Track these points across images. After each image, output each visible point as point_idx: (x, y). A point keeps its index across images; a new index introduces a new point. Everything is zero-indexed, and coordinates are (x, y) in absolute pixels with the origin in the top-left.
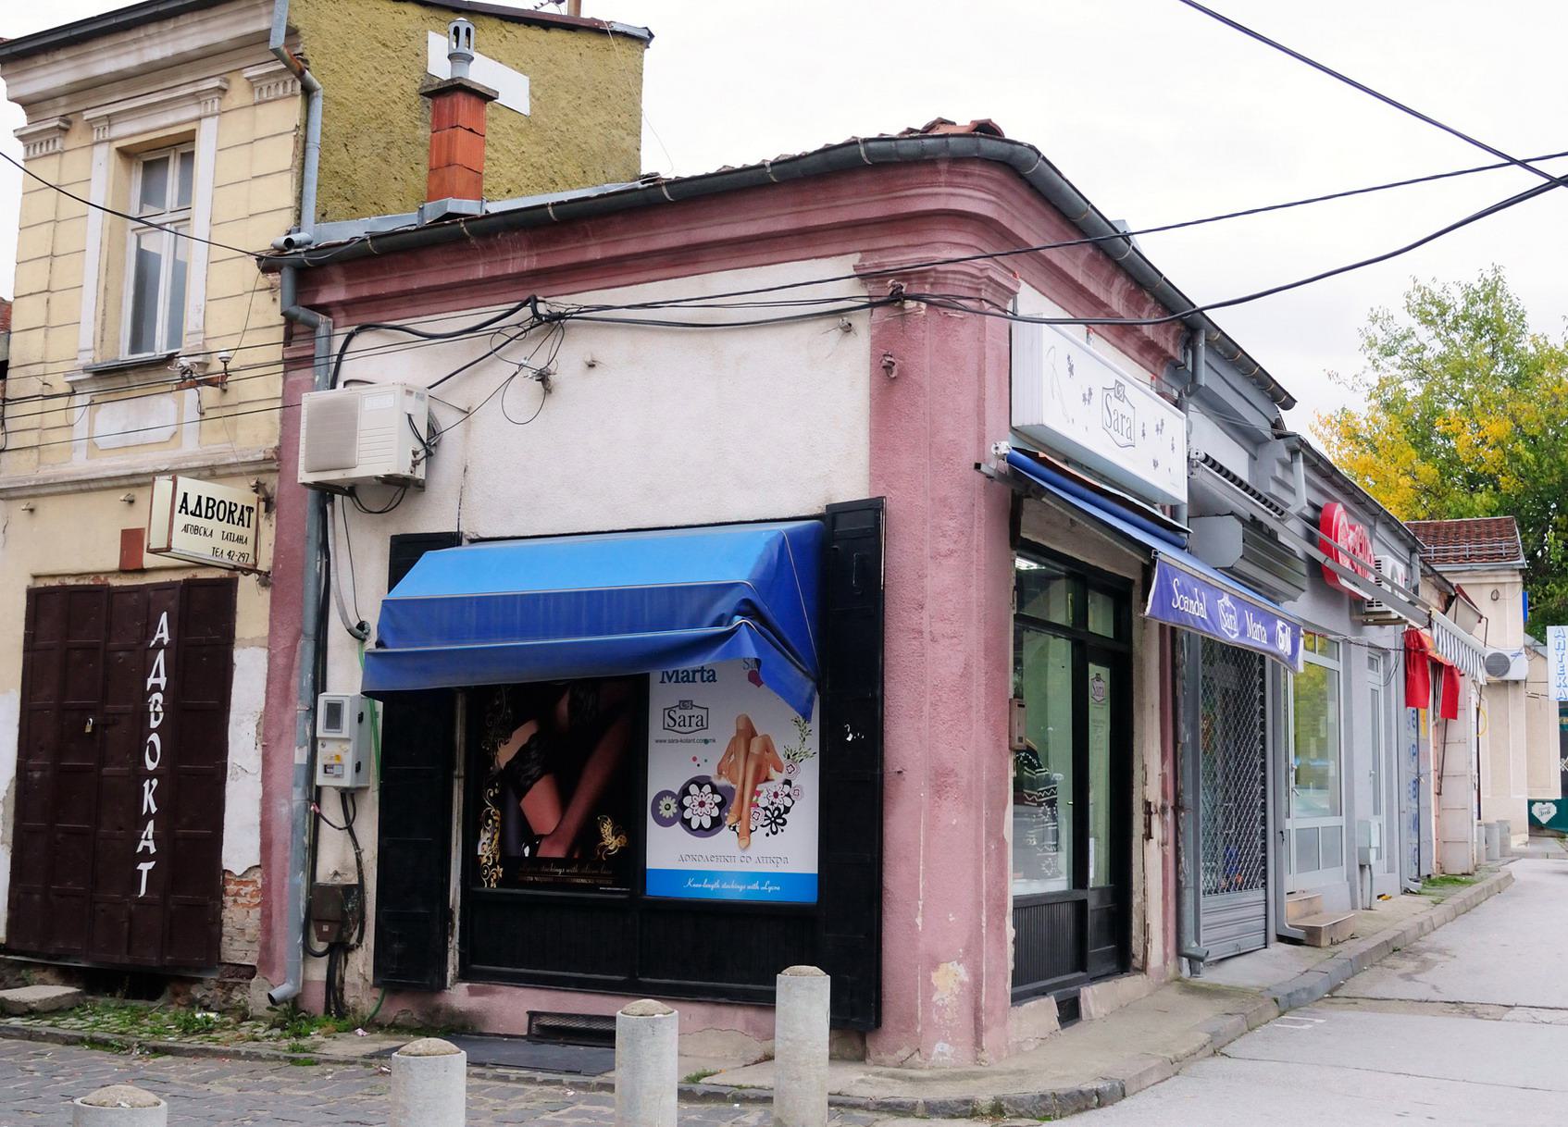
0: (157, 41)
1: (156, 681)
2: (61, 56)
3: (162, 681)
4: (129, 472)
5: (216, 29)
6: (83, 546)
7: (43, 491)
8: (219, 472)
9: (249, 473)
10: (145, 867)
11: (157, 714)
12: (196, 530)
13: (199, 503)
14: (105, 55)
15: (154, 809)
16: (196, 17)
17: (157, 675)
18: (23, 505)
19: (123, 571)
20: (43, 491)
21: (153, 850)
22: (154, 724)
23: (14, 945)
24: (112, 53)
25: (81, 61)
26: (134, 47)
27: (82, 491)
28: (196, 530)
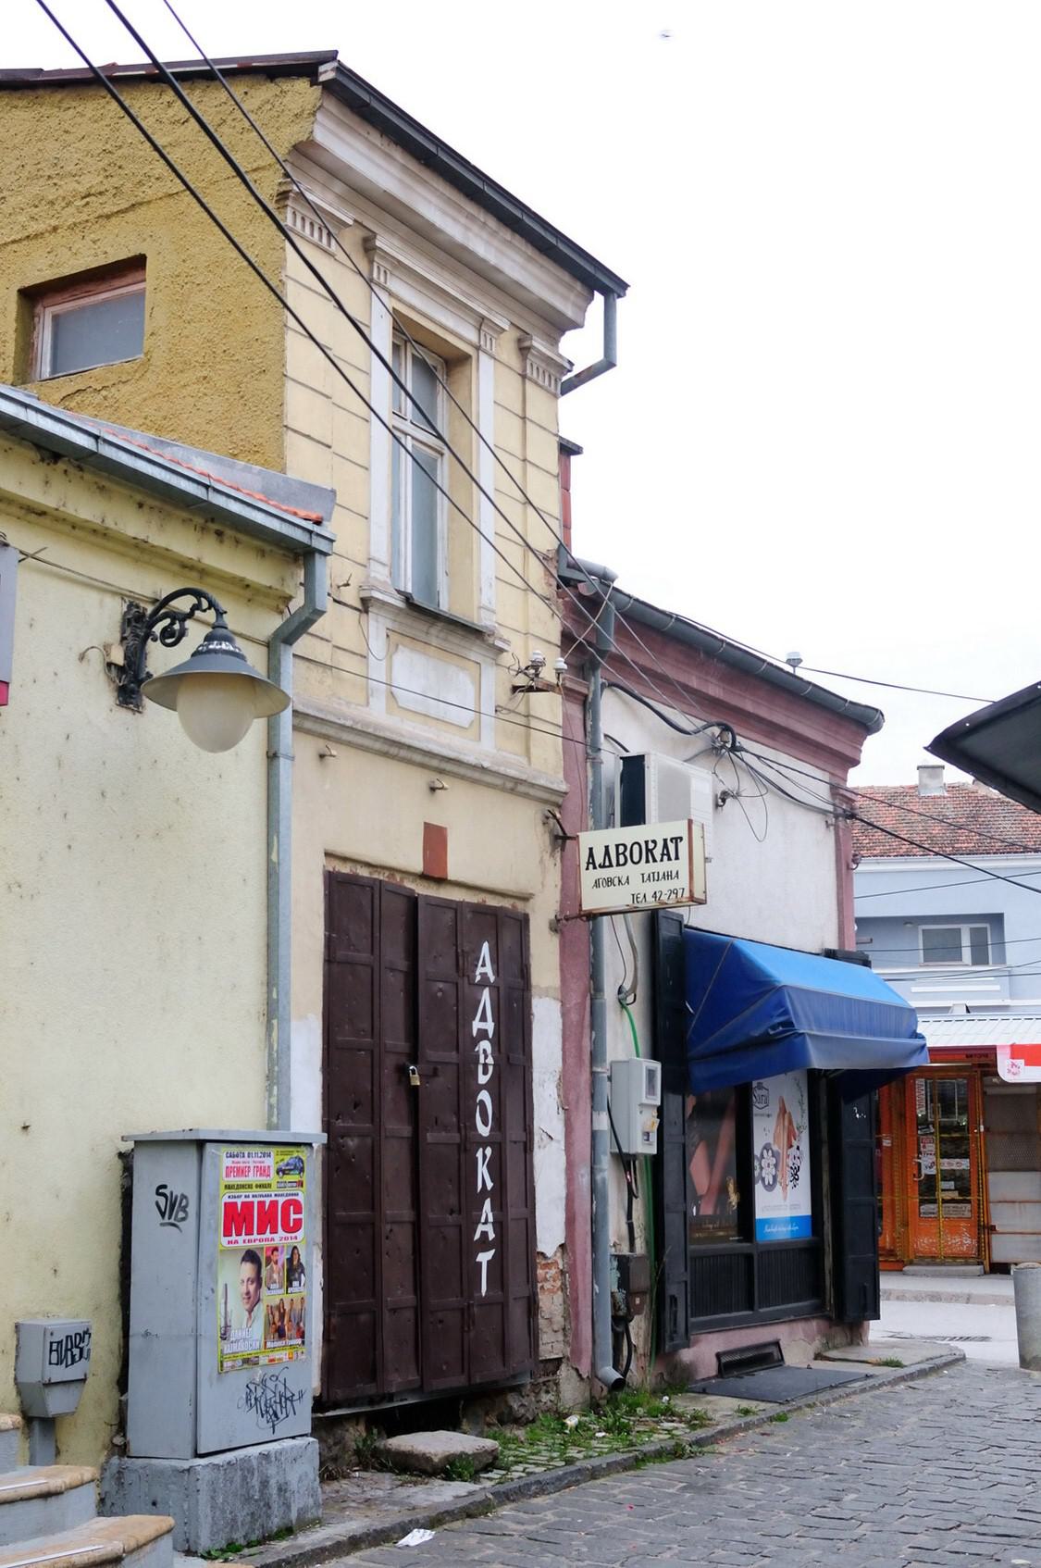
0: (485, 235)
1: (482, 1025)
2: (398, 154)
3: (490, 1026)
4: (452, 755)
5: (536, 278)
6: (380, 827)
7: (346, 736)
8: (521, 788)
9: (546, 802)
10: (484, 1258)
11: (485, 1065)
12: (609, 882)
13: (607, 852)
14: (434, 199)
15: (490, 1185)
16: (530, 250)
17: (483, 1019)
18: (321, 745)
19: (424, 877)
20: (346, 736)
21: (492, 1236)
22: (483, 1079)
23: (340, 1394)
24: (442, 205)
25: (408, 180)
26: (463, 220)
27: (385, 754)
28: (609, 882)
